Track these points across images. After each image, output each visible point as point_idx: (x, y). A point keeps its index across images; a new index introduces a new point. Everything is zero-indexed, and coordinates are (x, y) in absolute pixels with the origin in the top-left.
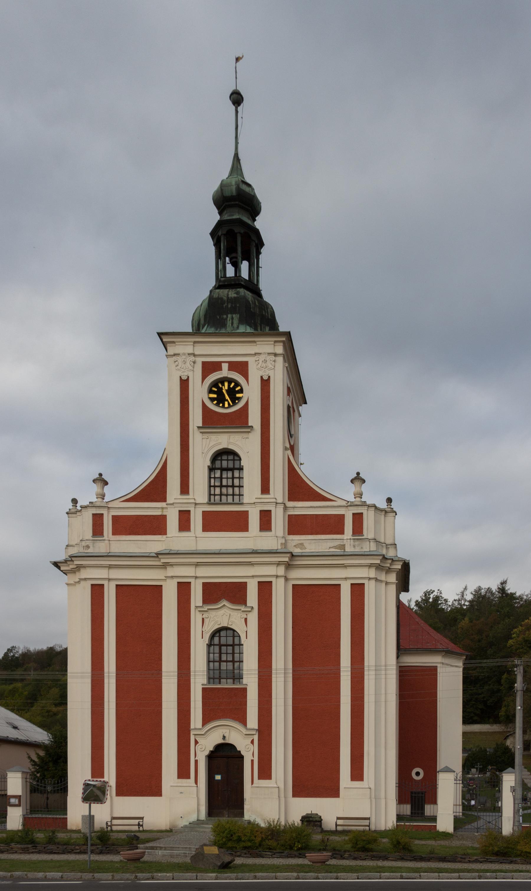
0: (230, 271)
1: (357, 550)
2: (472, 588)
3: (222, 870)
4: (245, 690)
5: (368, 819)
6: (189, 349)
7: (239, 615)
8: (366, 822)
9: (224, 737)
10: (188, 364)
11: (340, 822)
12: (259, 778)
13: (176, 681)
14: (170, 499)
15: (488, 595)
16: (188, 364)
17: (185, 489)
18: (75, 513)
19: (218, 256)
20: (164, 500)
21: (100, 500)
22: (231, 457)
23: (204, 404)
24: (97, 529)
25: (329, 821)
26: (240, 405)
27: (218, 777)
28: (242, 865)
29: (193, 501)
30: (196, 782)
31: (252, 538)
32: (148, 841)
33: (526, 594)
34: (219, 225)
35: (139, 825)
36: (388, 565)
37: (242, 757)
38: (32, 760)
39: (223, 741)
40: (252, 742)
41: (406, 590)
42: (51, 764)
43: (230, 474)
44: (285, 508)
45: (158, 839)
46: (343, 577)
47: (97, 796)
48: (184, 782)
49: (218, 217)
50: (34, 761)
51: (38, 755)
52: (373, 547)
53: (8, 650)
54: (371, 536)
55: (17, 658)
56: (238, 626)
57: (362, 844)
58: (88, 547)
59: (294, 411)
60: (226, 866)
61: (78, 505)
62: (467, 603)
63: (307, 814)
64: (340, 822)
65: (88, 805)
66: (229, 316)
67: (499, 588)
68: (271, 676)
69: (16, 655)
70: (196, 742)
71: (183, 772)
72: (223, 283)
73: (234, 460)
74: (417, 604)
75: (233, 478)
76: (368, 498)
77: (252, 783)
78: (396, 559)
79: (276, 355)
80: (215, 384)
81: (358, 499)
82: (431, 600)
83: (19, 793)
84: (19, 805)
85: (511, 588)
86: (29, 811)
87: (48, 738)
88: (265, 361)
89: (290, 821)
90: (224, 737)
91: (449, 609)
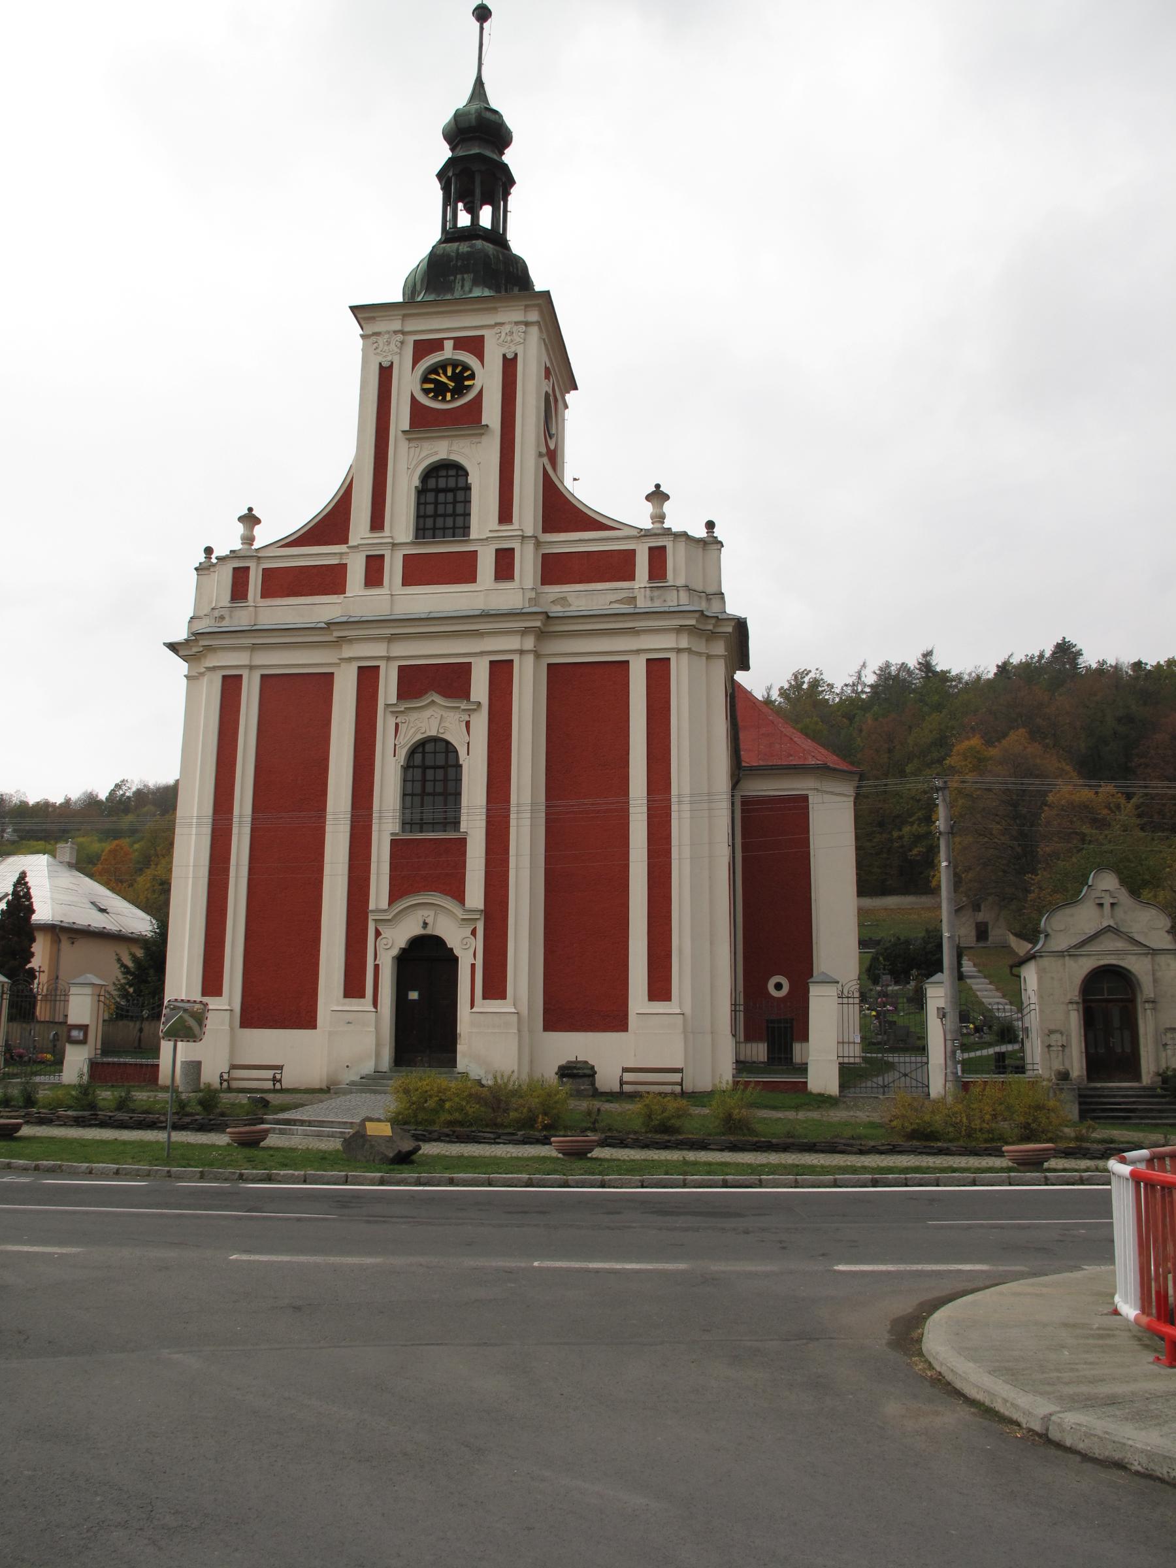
0: (464, 219)
1: (657, 605)
2: (874, 665)
3: (396, 1167)
4: (462, 842)
5: (680, 1070)
6: (397, 325)
7: (457, 716)
8: (677, 1077)
9: (425, 925)
10: (392, 346)
11: (628, 1077)
12: (484, 998)
13: (348, 828)
14: (354, 540)
15: (903, 674)
16: (392, 346)
17: (377, 522)
18: (207, 568)
19: (447, 201)
20: (344, 540)
21: (246, 547)
22: (452, 472)
23: (413, 398)
24: (239, 591)
25: (608, 1077)
26: (471, 395)
27: (414, 995)
28: (440, 1158)
29: (389, 540)
30: (375, 1004)
31: (484, 593)
32: (284, 1108)
33: (968, 671)
34: (450, 163)
35: (274, 1079)
36: (710, 627)
37: (456, 959)
38: (123, 965)
39: (422, 932)
40: (474, 933)
41: (745, 666)
42: (151, 972)
43: (450, 496)
44: (538, 544)
45: (302, 1105)
46: (635, 651)
47: (190, 1028)
48: (354, 1005)
49: (450, 154)
50: (126, 967)
51: (133, 956)
52: (683, 600)
53: (117, 786)
54: (681, 582)
55: (129, 798)
56: (456, 737)
57: (663, 1122)
58: (222, 618)
59: (556, 401)
60: (404, 1159)
61: (213, 556)
62: (867, 690)
63: (569, 1062)
64: (628, 1077)
65: (172, 1043)
66: (459, 277)
67: (920, 663)
68: (509, 816)
69: (128, 794)
70: (378, 934)
71: (353, 987)
72: (451, 234)
73: (457, 476)
74: (783, 693)
75: (455, 502)
76: (674, 522)
77: (472, 1007)
78: (725, 616)
79: (527, 324)
80: (434, 370)
81: (658, 525)
82: (805, 686)
83: (85, 1021)
84: (84, 1042)
85: (941, 663)
86: (99, 1052)
87: (150, 928)
88: (511, 333)
89: (537, 1076)
90: (425, 925)
91: (837, 700)
